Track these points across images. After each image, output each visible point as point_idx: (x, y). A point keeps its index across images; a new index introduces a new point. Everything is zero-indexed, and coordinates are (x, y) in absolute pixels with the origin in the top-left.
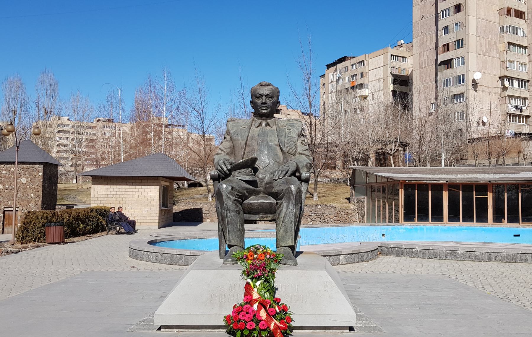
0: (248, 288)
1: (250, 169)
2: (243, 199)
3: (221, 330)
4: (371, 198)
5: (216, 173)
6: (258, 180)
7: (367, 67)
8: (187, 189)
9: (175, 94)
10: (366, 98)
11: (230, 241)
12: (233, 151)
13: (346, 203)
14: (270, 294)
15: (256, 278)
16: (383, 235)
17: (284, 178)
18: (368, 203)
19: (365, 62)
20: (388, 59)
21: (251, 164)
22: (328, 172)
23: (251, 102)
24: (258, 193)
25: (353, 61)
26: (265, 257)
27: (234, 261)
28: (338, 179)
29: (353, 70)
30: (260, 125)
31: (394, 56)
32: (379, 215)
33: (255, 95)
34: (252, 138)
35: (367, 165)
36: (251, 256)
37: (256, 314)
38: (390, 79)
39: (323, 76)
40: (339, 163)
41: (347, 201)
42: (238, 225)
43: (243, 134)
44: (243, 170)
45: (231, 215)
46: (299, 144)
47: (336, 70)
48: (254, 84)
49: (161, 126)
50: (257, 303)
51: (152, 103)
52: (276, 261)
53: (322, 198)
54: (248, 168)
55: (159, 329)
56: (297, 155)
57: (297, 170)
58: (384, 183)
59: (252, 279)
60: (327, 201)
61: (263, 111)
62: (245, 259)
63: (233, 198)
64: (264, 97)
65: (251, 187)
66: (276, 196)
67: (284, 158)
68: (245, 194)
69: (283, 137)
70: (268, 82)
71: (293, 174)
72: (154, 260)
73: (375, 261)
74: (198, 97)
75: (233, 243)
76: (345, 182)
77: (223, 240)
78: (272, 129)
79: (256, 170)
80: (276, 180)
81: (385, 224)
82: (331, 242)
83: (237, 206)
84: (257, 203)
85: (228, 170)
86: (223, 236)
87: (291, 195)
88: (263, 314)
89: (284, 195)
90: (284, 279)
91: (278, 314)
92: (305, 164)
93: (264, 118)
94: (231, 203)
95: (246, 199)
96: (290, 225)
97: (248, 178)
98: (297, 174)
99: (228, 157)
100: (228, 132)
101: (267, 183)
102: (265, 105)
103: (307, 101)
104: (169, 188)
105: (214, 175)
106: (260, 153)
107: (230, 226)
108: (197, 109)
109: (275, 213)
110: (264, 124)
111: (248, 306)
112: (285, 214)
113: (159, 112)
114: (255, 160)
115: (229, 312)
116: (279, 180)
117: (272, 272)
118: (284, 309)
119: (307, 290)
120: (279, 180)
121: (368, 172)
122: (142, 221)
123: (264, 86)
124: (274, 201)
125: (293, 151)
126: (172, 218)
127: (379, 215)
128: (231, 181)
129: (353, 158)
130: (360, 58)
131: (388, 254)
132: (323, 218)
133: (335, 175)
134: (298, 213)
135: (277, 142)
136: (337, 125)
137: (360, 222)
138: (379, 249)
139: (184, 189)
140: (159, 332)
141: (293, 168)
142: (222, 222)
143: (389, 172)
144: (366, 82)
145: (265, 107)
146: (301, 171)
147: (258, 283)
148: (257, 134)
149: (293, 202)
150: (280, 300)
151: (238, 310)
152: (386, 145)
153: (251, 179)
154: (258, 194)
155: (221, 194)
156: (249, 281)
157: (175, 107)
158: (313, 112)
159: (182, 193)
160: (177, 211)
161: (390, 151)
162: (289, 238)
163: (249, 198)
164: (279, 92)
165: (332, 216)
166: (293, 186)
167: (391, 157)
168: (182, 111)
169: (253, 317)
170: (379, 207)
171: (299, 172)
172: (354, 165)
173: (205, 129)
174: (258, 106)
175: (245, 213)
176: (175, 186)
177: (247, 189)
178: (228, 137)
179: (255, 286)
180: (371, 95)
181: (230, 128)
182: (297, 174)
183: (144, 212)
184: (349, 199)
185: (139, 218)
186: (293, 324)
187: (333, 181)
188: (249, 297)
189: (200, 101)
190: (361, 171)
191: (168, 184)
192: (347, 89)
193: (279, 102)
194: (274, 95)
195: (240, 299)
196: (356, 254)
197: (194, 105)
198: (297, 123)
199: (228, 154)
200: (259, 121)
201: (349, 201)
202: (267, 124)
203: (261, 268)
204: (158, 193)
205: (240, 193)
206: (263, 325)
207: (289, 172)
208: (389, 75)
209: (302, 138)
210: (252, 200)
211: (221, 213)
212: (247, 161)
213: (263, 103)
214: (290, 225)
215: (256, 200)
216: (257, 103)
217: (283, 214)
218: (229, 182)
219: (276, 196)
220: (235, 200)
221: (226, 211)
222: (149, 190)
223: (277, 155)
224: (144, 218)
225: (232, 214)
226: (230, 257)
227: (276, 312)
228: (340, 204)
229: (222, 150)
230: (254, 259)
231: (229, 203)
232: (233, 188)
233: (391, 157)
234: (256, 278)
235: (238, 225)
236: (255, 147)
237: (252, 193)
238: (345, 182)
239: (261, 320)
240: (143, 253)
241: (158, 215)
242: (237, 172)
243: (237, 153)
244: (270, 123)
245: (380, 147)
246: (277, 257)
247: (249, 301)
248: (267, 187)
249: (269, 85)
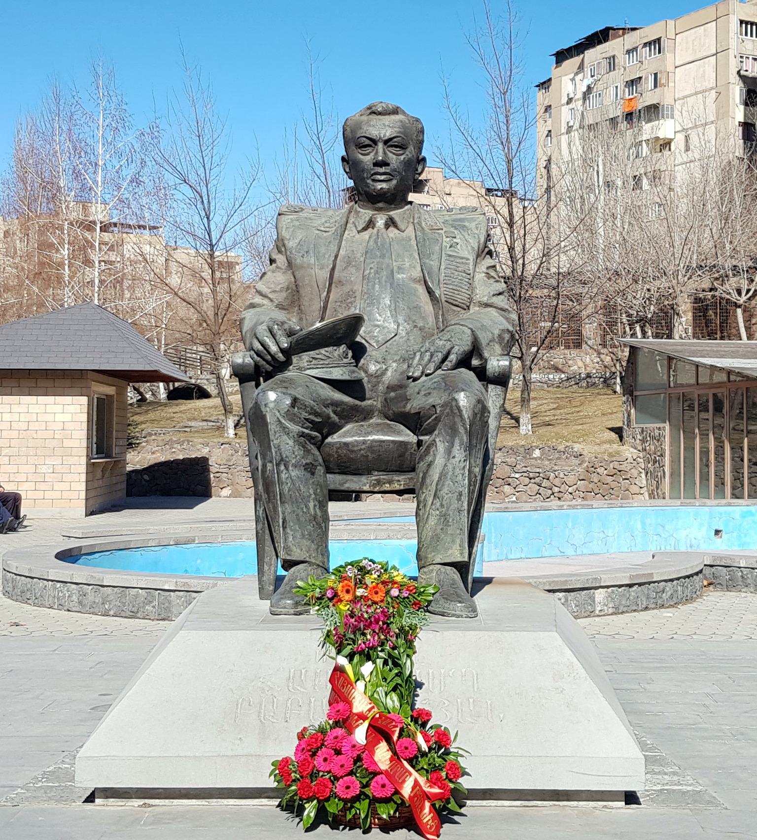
0: (340, 683)
1: (343, 348)
2: (325, 431)
3: (265, 801)
4: (683, 427)
5: (248, 360)
6: (365, 380)
7: (669, 56)
8: (165, 405)
9: (127, 139)
10: (666, 144)
11: (287, 549)
12: (294, 298)
13: (610, 442)
14: (401, 697)
15: (361, 653)
16: (717, 532)
17: (439, 372)
18: (675, 441)
19: (665, 43)
20: (731, 35)
21: (346, 335)
22: (559, 355)
23: (343, 159)
24: (365, 415)
25: (631, 39)
26: (387, 593)
27: (301, 607)
28: (589, 376)
29: (629, 68)
30: (371, 224)
31: (747, 23)
32: (705, 477)
33: (355, 141)
34: (349, 262)
35: (670, 336)
36: (348, 592)
37: (361, 759)
38: (737, 91)
39: (545, 85)
40: (590, 330)
41: (614, 436)
42: (311, 505)
43: (323, 250)
44: (323, 351)
45: (291, 477)
46: (480, 277)
47: (581, 67)
48: (351, 108)
49: (89, 226)
50: (366, 724)
51: (64, 163)
52: (417, 605)
53: (543, 430)
54: (337, 344)
55: (90, 799)
56: (474, 309)
57: (475, 349)
58: (719, 385)
59: (351, 657)
60: (559, 436)
61: (379, 186)
62: (331, 599)
63: (295, 428)
64: (380, 145)
65: (346, 399)
66: (415, 422)
67: (437, 318)
68: (329, 417)
69: (435, 257)
70: (392, 103)
71: (464, 362)
72: (74, 605)
73: (695, 604)
74: (193, 144)
75: (296, 555)
76: (607, 382)
77: (269, 548)
78: (404, 234)
79: (358, 351)
80: (415, 379)
81: (723, 501)
82: (570, 551)
83: (308, 451)
84: (364, 442)
85: (282, 351)
86: (268, 537)
87: (457, 419)
88: (382, 755)
89: (437, 420)
90: (442, 656)
91: (424, 754)
92: (496, 332)
93: (380, 205)
94: (291, 442)
95: (331, 433)
96: (455, 505)
97: (337, 374)
98: (475, 362)
99: (281, 316)
100: (280, 245)
101: (390, 388)
102: (382, 170)
103: (499, 154)
104: (115, 399)
105: (243, 366)
106: (371, 304)
107: (288, 508)
108: (193, 178)
109: (413, 470)
110: (380, 222)
111: (340, 732)
112: (443, 475)
113: (82, 189)
114: (356, 322)
115: (288, 749)
116: (424, 378)
117: (408, 636)
118: (442, 740)
119: (508, 694)
120: (424, 378)
121: (672, 354)
122: (39, 495)
123: (380, 114)
124: (408, 436)
125: (462, 298)
126: (124, 485)
127: (705, 477)
128: (291, 381)
129: (629, 316)
130: (650, 33)
131: (731, 585)
132: (545, 483)
133: (580, 364)
134: (477, 470)
135: (417, 273)
136: (584, 223)
137: (652, 496)
138: (707, 571)
139: (157, 404)
140: (89, 806)
141: (462, 345)
142: (264, 496)
143: (734, 355)
144: (667, 101)
145: (384, 175)
146: (486, 354)
147: (367, 668)
148: (361, 249)
149: (465, 438)
150: (429, 715)
151: (311, 744)
152: (723, 279)
153: (346, 377)
154: (365, 419)
155: (263, 417)
156: (342, 661)
157: (128, 173)
158: (517, 186)
159: (151, 416)
160: (138, 467)
161: (734, 297)
162: (453, 541)
163: (340, 428)
164: (422, 131)
165: (571, 479)
166: (462, 394)
167: (739, 311)
168: (150, 186)
169: (355, 763)
170: (705, 453)
171: (481, 356)
172: (633, 335)
173: (215, 236)
174: (363, 171)
175: (329, 470)
176: (132, 396)
177: (335, 404)
178: (281, 259)
179: (359, 677)
180: (680, 138)
181: (285, 234)
182: (475, 362)
183: (43, 469)
184: (618, 431)
185: (31, 486)
186: (465, 783)
187: (575, 380)
188: (341, 706)
189: (199, 156)
190: (652, 352)
191: (111, 390)
192: (613, 121)
193: (424, 159)
194: (409, 141)
195: (317, 714)
196: (640, 585)
197: (183, 168)
198: (473, 220)
199: (280, 307)
200: (366, 213)
201: (621, 438)
202: (391, 223)
203: (374, 626)
204: (84, 417)
205: (316, 414)
206: (383, 786)
207: (453, 357)
208: (734, 78)
209: (488, 261)
210: (348, 435)
211: (264, 471)
212: (334, 326)
213: (377, 164)
214: (455, 505)
215: (359, 435)
216: (361, 162)
217: (435, 474)
218: (287, 385)
219: (415, 422)
220: (303, 435)
221: (278, 465)
222: (59, 408)
223: (417, 308)
224: (43, 486)
225: (294, 473)
226: (288, 594)
227: (419, 749)
228: (596, 445)
229: (265, 296)
230: (355, 600)
231: (285, 443)
232: (295, 400)
233: (739, 311)
234: (361, 653)
235: (311, 505)
236: (358, 287)
237: (348, 415)
238: (607, 382)
239: (376, 774)
240: (42, 584)
241: (83, 477)
242: (306, 356)
243: (305, 302)
244: (397, 219)
245: (706, 285)
246: (420, 594)
247: (344, 719)
248: (392, 399)
249: (395, 111)
